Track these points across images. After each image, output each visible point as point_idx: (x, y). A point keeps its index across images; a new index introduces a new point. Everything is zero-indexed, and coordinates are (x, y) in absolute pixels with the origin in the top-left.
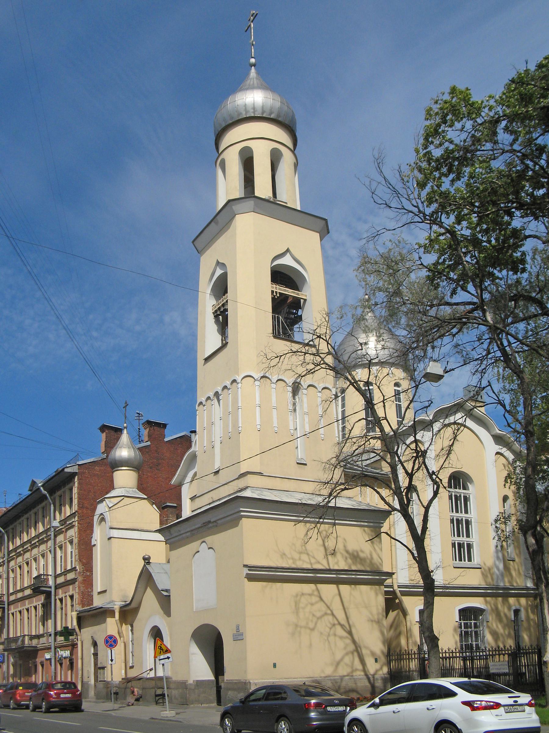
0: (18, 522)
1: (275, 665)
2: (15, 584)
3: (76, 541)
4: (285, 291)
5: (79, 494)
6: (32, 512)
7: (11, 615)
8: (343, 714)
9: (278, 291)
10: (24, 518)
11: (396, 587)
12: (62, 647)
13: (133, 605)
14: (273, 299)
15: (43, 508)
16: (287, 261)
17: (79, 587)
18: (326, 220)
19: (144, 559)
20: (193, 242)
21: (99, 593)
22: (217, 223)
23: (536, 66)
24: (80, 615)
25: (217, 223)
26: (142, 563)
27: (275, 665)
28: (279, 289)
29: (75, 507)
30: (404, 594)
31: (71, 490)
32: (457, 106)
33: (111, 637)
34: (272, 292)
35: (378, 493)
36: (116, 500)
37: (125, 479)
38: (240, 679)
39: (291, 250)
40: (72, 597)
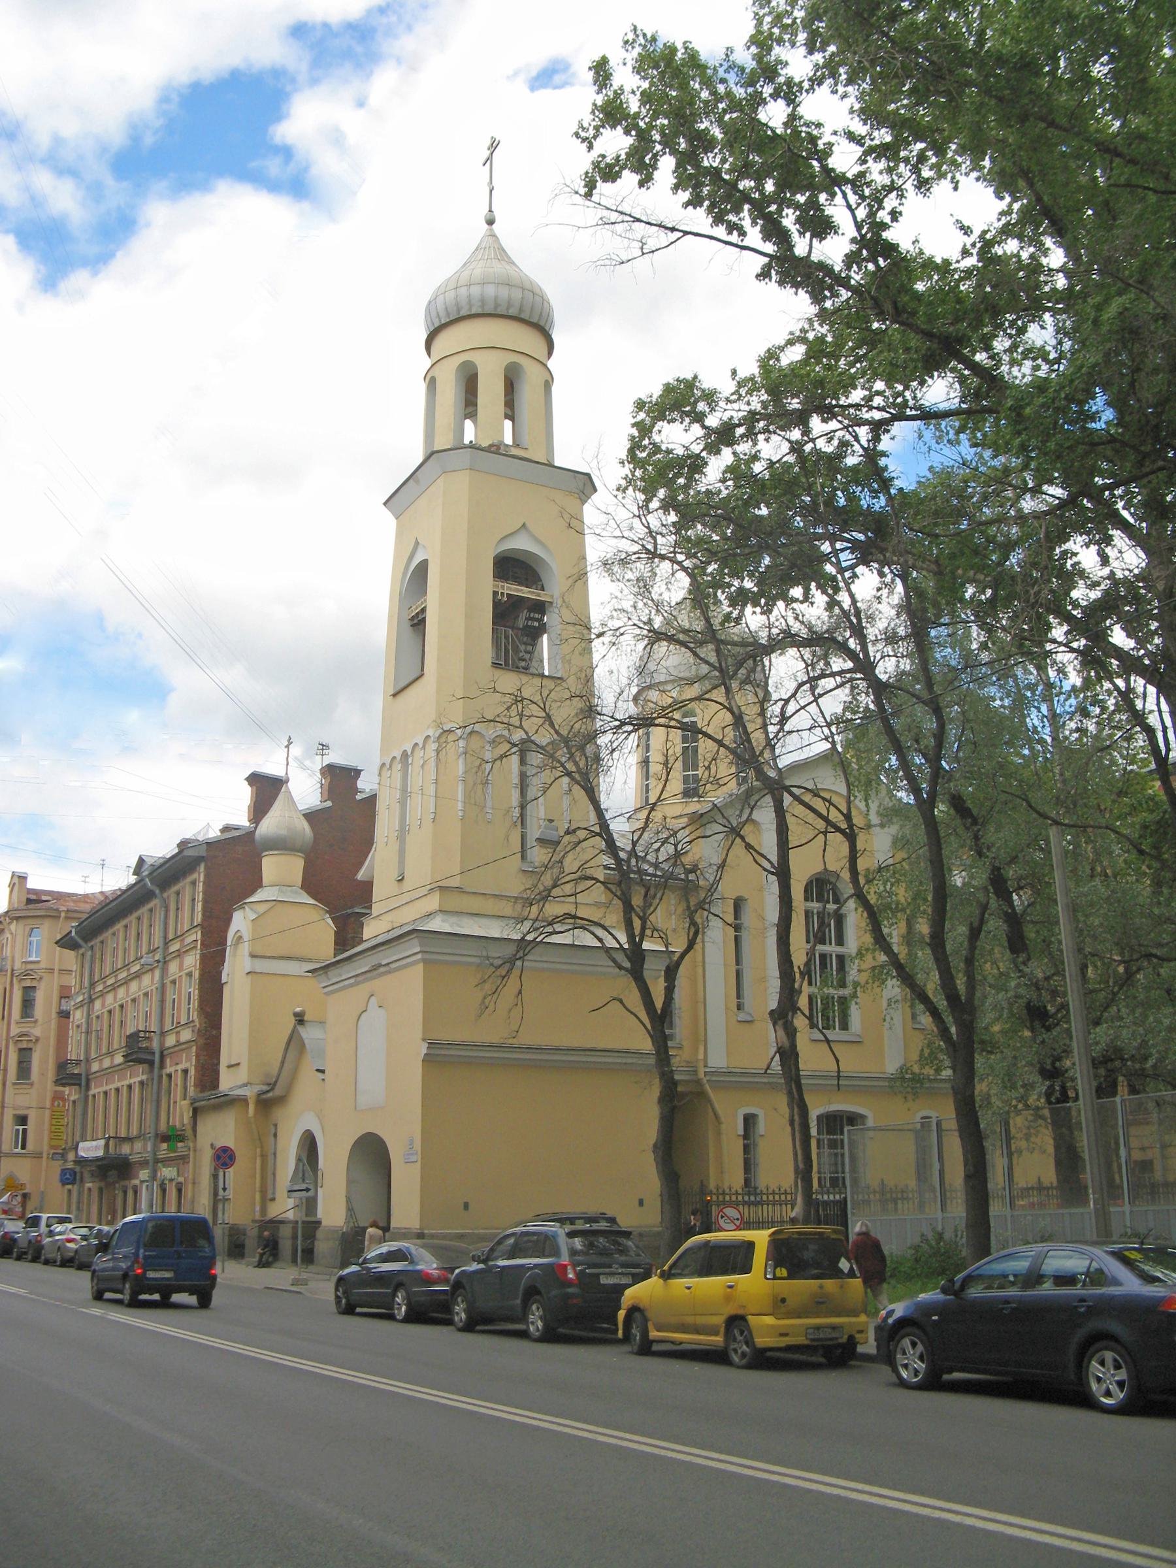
0: (111, 931)
1: (466, 1206)
2: (99, 1047)
3: (196, 975)
4: (518, 590)
5: (204, 893)
6: (133, 918)
7: (90, 1098)
8: (620, 1289)
9: (506, 592)
10: (119, 926)
11: (701, 1075)
12: (166, 1162)
13: (278, 1092)
14: (496, 604)
15: (126, 926)
16: (522, 543)
17: (197, 1056)
18: (588, 475)
19: (296, 1015)
20: (385, 504)
21: (229, 1067)
22: (417, 482)
23: (102, 893)
24: (197, 1104)
25: (417, 482)
26: (292, 1020)
27: (466, 1206)
28: (508, 588)
29: (198, 918)
30: (716, 1085)
31: (194, 883)
32: (681, 400)
33: (225, 1149)
34: (495, 593)
35: (593, 934)
36: (262, 908)
37: (280, 873)
38: (584, 1210)
39: (528, 524)
40: (186, 1071)
